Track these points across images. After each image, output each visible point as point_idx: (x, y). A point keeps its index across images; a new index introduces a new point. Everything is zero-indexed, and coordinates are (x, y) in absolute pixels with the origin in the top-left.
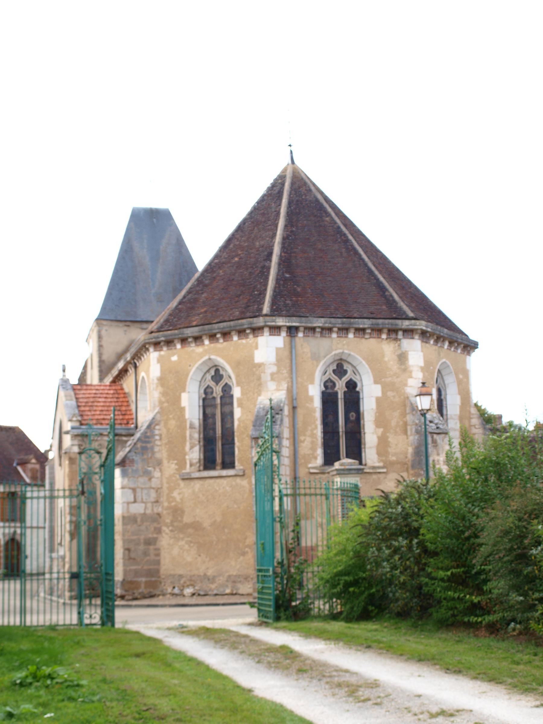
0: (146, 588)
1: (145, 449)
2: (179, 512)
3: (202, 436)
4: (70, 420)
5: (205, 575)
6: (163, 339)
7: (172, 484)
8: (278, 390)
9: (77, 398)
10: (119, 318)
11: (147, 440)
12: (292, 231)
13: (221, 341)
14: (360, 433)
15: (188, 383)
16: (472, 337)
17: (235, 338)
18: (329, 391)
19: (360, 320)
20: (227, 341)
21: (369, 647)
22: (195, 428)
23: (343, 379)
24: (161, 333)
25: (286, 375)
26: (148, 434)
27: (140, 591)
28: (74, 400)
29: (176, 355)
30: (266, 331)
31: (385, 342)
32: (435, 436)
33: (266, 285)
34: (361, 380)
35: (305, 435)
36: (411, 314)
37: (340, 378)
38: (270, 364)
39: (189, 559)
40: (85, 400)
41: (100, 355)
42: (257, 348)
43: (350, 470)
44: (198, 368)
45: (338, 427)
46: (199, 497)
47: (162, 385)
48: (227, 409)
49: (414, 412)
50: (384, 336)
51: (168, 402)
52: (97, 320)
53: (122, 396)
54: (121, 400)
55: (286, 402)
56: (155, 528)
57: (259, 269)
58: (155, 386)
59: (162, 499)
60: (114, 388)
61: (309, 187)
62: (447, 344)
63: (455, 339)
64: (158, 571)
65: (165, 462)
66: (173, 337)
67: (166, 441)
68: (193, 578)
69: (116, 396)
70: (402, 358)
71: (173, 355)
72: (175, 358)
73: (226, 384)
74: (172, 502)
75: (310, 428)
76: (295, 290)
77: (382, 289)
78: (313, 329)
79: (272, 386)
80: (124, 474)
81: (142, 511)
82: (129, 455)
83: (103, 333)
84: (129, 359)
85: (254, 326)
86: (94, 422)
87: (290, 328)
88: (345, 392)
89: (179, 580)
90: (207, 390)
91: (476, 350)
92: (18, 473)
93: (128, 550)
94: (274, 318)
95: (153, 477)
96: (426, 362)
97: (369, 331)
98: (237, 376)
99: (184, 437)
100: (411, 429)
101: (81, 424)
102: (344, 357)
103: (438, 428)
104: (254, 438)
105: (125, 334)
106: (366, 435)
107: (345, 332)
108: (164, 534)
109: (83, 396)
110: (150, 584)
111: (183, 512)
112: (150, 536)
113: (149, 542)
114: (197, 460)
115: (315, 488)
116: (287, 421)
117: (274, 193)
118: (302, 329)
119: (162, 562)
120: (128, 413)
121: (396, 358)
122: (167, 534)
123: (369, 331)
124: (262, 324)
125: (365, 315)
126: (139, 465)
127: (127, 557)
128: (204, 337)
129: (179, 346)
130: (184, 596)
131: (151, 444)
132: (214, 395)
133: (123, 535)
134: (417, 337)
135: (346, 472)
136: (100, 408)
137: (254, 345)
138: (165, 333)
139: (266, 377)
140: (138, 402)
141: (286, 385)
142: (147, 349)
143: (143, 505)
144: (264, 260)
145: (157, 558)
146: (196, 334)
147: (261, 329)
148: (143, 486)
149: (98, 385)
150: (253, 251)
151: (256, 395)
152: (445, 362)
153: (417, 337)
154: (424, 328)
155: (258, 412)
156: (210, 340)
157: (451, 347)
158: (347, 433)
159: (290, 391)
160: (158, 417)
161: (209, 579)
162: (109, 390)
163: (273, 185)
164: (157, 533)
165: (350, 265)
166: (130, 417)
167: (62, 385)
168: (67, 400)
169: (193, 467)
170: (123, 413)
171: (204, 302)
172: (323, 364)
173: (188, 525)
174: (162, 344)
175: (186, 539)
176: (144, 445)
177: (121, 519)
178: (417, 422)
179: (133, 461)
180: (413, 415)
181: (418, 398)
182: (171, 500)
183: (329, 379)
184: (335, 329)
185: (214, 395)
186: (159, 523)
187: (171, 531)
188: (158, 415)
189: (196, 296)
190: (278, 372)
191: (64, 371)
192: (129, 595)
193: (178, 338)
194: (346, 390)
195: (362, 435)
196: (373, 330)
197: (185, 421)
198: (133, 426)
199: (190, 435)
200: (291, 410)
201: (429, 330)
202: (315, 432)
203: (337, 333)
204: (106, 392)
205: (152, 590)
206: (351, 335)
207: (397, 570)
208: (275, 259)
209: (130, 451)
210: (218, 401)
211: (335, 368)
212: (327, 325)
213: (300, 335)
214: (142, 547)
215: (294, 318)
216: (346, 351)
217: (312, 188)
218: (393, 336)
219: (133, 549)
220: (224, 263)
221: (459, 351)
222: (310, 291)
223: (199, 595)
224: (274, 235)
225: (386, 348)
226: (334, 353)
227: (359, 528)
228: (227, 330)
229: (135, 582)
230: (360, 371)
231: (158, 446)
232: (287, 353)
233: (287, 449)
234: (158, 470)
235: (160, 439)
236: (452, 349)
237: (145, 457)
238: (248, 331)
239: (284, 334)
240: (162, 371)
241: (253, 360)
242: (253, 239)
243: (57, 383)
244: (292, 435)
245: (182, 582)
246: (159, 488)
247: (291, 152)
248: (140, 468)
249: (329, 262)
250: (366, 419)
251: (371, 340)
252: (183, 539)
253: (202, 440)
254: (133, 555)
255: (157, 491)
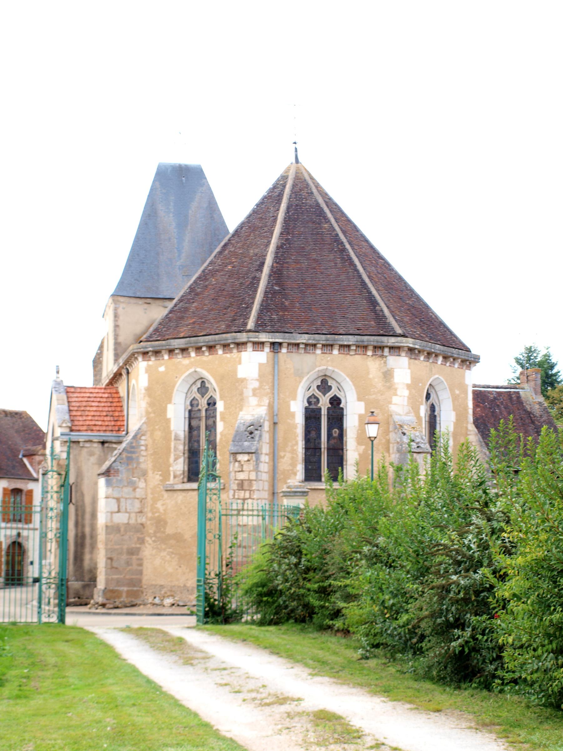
0: (127, 597)
1: (130, 460)
2: (162, 523)
3: (187, 448)
4: (60, 426)
5: (185, 586)
6: (150, 349)
7: (156, 495)
8: (259, 405)
9: (69, 402)
10: (138, 294)
11: (132, 450)
12: (287, 240)
13: (207, 354)
14: (342, 449)
15: (174, 395)
16: (474, 351)
17: (220, 352)
18: (313, 407)
19: (345, 337)
20: (213, 354)
21: (244, 640)
22: (179, 440)
23: (327, 395)
24: (149, 343)
25: (269, 391)
26: (134, 445)
27: (122, 600)
28: (66, 404)
29: (163, 365)
30: (250, 347)
31: (370, 359)
32: (415, 455)
33: (254, 298)
34: (345, 397)
35: (285, 451)
36: (399, 331)
37: (324, 394)
38: (252, 380)
39: (170, 570)
40: (78, 404)
41: (116, 336)
42: (240, 363)
43: (296, 492)
44: (183, 380)
45: (320, 443)
46: (181, 509)
47: (150, 396)
48: (210, 422)
49: (396, 431)
50: (370, 353)
51: (154, 413)
52: (113, 295)
53: (117, 400)
54: (115, 404)
55: (267, 418)
56: (138, 538)
57: (250, 280)
58: (142, 396)
59: (146, 510)
60: (109, 391)
61: (311, 189)
62: (440, 359)
63: (449, 354)
64: (140, 581)
65: (150, 473)
66: (161, 348)
67: (152, 452)
68: (174, 589)
69: (111, 400)
70: (388, 375)
71: (161, 365)
72: (162, 369)
73: (211, 396)
74: (156, 512)
75: (290, 444)
76: (283, 303)
77: (373, 303)
78: (297, 345)
79: (253, 401)
80: (109, 484)
81: (126, 522)
82: (114, 465)
83: (120, 311)
84: (121, 364)
85: (237, 341)
86: (85, 428)
87: (273, 344)
88: (328, 409)
89: (160, 591)
90: (193, 402)
91: (477, 364)
92: (25, 465)
93: (111, 559)
94: (257, 334)
95: (138, 487)
96: (413, 378)
97: (353, 348)
98: (221, 390)
99: (169, 449)
100: (393, 447)
101: (72, 430)
102: (328, 374)
103: (418, 447)
104: (232, 453)
105: (145, 313)
106: (348, 452)
107: (329, 348)
108: (147, 545)
109: (76, 399)
110: (130, 594)
111: (166, 523)
112: (133, 546)
113: (132, 552)
114: (181, 472)
115: (258, 510)
116: (266, 437)
117: (273, 197)
118: (285, 345)
119: (145, 572)
120: (121, 419)
121: (381, 375)
122: (150, 544)
123: (353, 348)
124: (245, 340)
125: (351, 332)
126: (123, 475)
127: (109, 567)
128: (190, 350)
129: (166, 357)
130: (164, 606)
131: (137, 455)
132: (200, 407)
133: (106, 545)
134: (403, 354)
135: (291, 494)
136: (92, 413)
137: (238, 359)
138: (153, 343)
139: (248, 392)
140: (130, 409)
141: (268, 401)
142: (136, 358)
143: (127, 515)
144: (257, 270)
145: (140, 568)
146: (183, 346)
147: (244, 344)
148: (127, 497)
149: (92, 388)
150: (247, 259)
151: (238, 409)
152: (438, 378)
153: (403, 354)
154: (411, 346)
155: (238, 427)
156: (196, 353)
157: (446, 362)
158: (329, 449)
159: (271, 407)
160: (145, 428)
161: (188, 590)
162: (104, 393)
163: (275, 187)
164: (140, 544)
165: (343, 277)
166: (122, 423)
167: (55, 388)
168: (58, 404)
169: (177, 479)
170: (116, 419)
171: (193, 312)
172: (306, 381)
173: (169, 537)
174: (150, 354)
175: (168, 550)
176: (129, 455)
177: (104, 529)
178: (399, 440)
179: (117, 471)
180: (396, 433)
181: (366, 425)
182: (155, 510)
183: (313, 394)
184: (319, 346)
185: (200, 407)
186: (142, 534)
187: (154, 541)
188: (145, 426)
189: (187, 305)
190: (260, 387)
191: (58, 372)
192: (110, 603)
193: (165, 349)
194: (330, 406)
195: (345, 451)
196: (358, 346)
197: (170, 432)
198: (124, 433)
199: (175, 447)
200: (272, 426)
201: (417, 347)
202: (295, 448)
203: (322, 349)
204: (100, 395)
205: (133, 599)
206: (336, 352)
207: (288, 583)
208: (266, 270)
209: (115, 461)
210: (203, 413)
211: (319, 384)
212: (310, 342)
213: (284, 350)
214: (124, 557)
215: (277, 334)
216: (330, 368)
217: (314, 190)
218: (379, 352)
219: (115, 558)
220: (217, 271)
221: (456, 365)
222: (297, 305)
223: (178, 605)
224: (269, 242)
225: (371, 364)
226: (317, 369)
227: (267, 547)
228: (211, 344)
229: (117, 591)
230: (344, 388)
231: (143, 456)
232: (269, 369)
233: (266, 465)
234: (142, 480)
235: (146, 450)
236: (448, 364)
237: (130, 467)
238: (232, 346)
239: (267, 349)
240: (150, 381)
241: (236, 375)
242: (248, 247)
243: (51, 384)
244: (272, 451)
245: (163, 592)
246: (143, 499)
247: (296, 149)
248: (125, 478)
249: (322, 273)
250: (348, 436)
251: (356, 356)
252: (164, 550)
253: (186, 452)
254: (115, 565)
255: (141, 502)
